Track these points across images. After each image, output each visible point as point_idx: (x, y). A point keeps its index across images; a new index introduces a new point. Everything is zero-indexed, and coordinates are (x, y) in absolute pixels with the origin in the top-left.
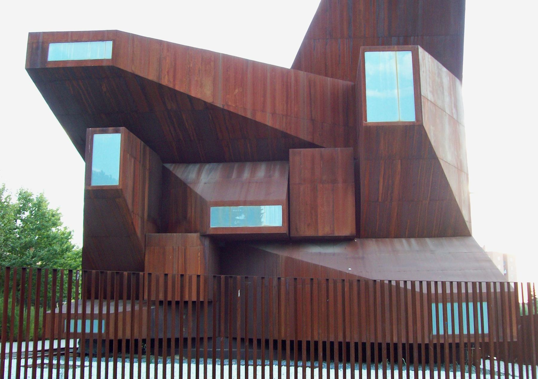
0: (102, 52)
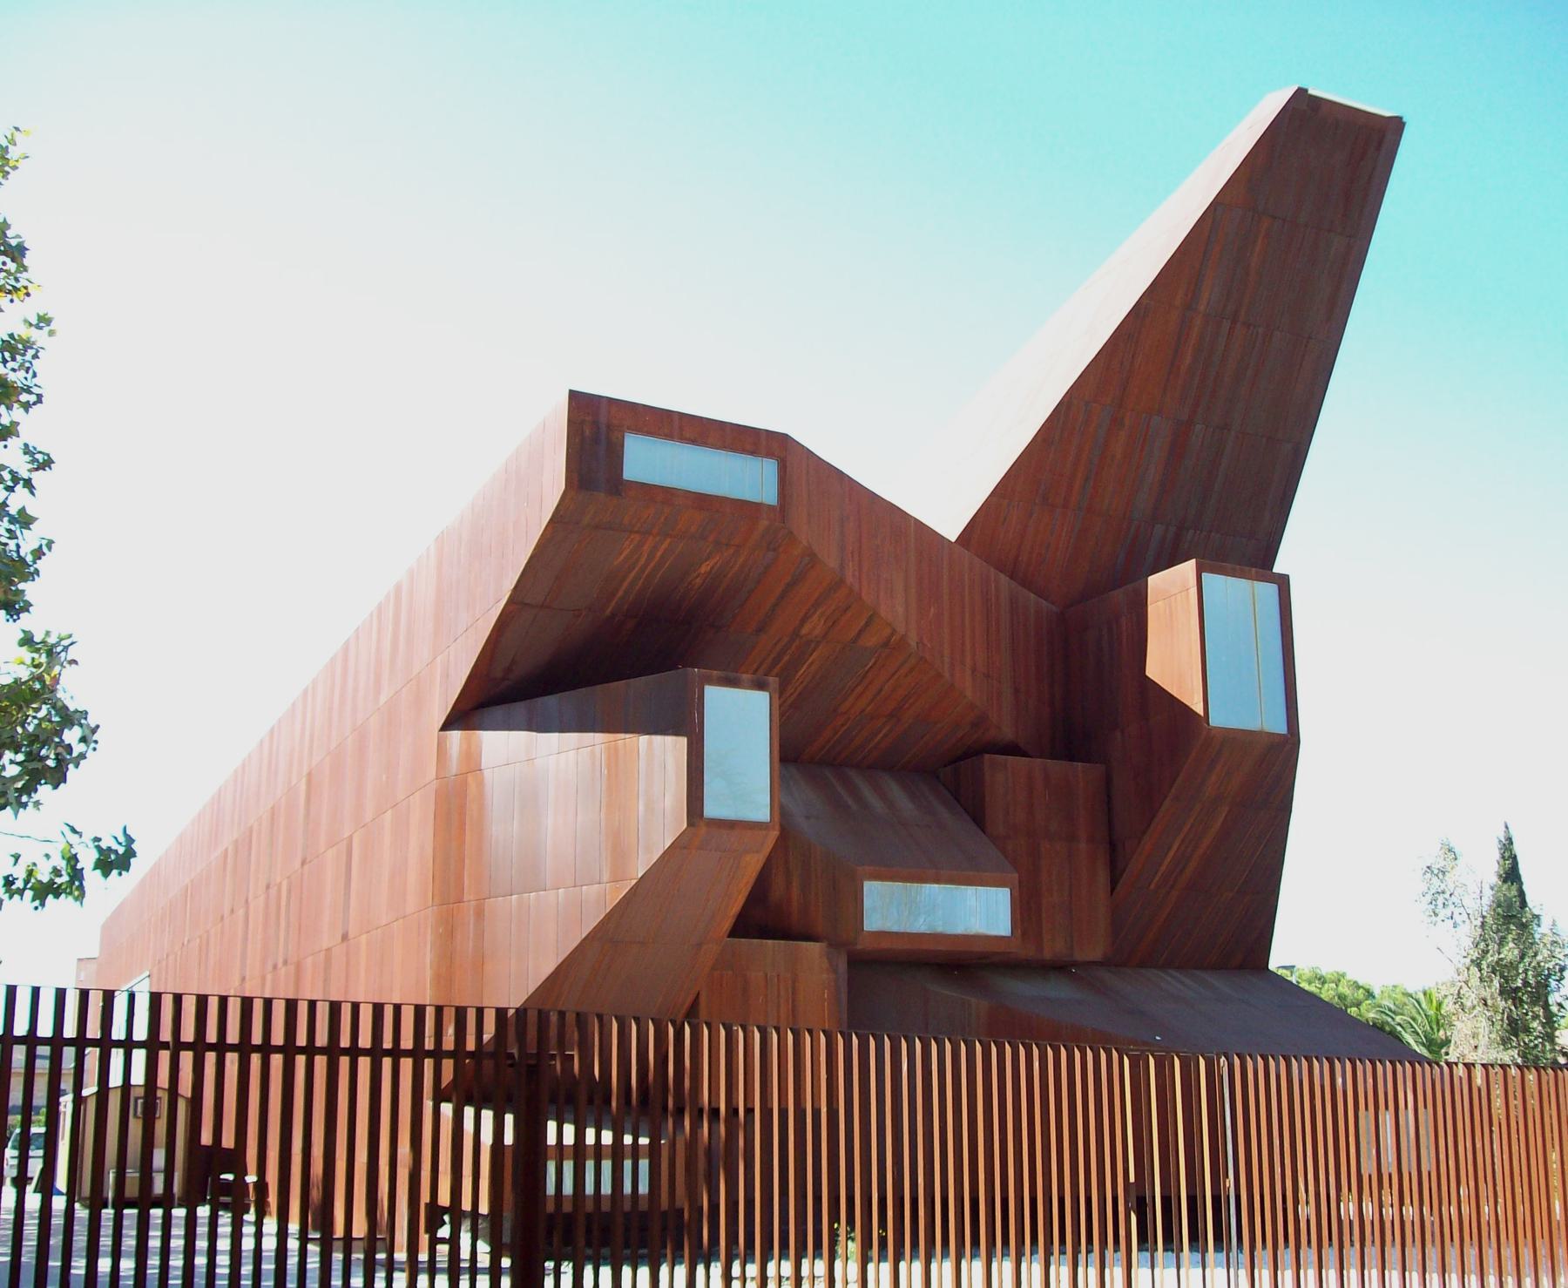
0: (751, 480)
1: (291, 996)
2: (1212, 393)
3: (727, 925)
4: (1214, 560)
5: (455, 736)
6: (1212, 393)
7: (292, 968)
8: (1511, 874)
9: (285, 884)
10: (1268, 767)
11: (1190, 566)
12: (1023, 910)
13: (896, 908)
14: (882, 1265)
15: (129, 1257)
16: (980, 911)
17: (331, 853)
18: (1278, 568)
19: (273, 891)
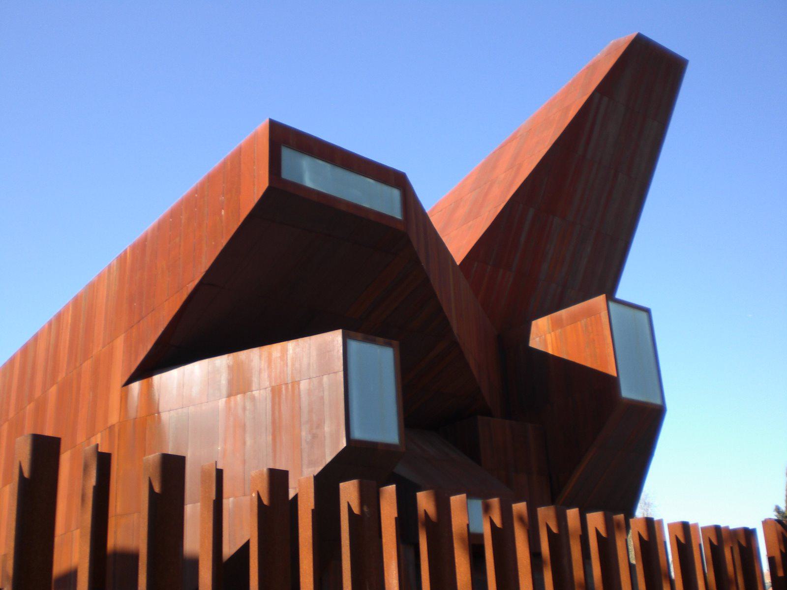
0: (384, 201)
5: (136, 386)
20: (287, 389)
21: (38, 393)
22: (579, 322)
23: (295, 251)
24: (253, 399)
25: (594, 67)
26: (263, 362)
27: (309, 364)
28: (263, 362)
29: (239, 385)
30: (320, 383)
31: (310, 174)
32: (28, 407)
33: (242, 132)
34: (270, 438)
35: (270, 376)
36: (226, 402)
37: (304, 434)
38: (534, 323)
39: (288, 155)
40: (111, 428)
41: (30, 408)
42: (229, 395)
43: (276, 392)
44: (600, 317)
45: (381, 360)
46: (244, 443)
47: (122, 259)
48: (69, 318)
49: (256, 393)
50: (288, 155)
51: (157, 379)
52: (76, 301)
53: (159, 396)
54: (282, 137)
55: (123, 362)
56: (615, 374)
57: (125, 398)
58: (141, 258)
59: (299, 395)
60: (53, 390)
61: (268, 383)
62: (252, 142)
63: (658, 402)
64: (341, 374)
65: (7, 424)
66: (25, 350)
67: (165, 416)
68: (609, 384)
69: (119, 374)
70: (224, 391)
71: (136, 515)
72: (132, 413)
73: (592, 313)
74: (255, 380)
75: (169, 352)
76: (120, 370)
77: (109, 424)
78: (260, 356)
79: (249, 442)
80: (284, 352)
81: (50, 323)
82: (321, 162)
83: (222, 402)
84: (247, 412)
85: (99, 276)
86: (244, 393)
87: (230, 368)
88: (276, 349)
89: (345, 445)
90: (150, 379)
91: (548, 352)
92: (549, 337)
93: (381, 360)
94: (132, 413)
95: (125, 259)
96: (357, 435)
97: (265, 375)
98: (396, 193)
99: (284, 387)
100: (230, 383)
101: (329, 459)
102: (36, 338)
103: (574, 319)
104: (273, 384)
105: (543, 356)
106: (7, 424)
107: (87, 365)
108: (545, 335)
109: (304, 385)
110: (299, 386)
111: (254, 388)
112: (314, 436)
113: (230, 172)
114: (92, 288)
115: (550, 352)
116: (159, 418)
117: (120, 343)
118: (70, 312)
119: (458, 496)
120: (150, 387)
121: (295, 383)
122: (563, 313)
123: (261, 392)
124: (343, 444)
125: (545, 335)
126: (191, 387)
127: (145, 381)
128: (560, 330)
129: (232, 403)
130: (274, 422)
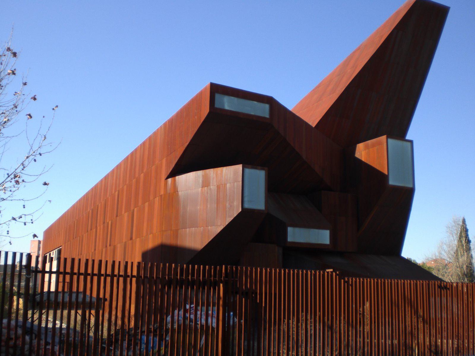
0: (262, 111)
1: (66, 257)
2: (389, 82)
3: (33, 238)
4: (390, 135)
5: (170, 180)
6: (389, 82)
7: (112, 247)
8: (25, 182)
9: (110, 222)
10: (404, 198)
11: (384, 137)
12: (333, 237)
13: (296, 235)
14: (367, 303)
15: (64, 328)
16: (323, 237)
17: (126, 214)
18: (408, 137)
19: (106, 225)
20: (222, 186)
21: (137, 175)
22: (375, 147)
23: (225, 130)
24: (211, 189)
25: (398, 13)
26: (214, 175)
27: (230, 177)
28: (214, 175)
29: (206, 183)
30: (234, 185)
31: (228, 104)
32: (133, 181)
33: (199, 85)
34: (216, 205)
35: (217, 181)
36: (201, 190)
37: (227, 204)
38: (358, 145)
39: (217, 96)
40: (161, 196)
41: (134, 181)
42: (202, 187)
43: (218, 187)
44: (384, 146)
45: (259, 176)
46: (207, 207)
47: (165, 124)
48: (147, 146)
49: (212, 187)
50: (217, 96)
51: (177, 177)
52: (150, 138)
53: (178, 185)
54: (216, 90)
55: (165, 171)
56: (387, 174)
57: (166, 184)
58: (172, 126)
59: (226, 189)
60: (142, 175)
61: (216, 183)
62: (206, 88)
63: (411, 186)
64: (241, 182)
65: (126, 186)
66: (132, 154)
67: (180, 193)
68: (382, 178)
69: (164, 175)
70: (201, 186)
71: (169, 231)
72: (168, 191)
73: (380, 143)
74: (211, 182)
75: (181, 168)
76: (164, 173)
77: (161, 194)
78: (214, 172)
79: (209, 206)
80: (222, 171)
81: (141, 145)
82: (233, 98)
83: (200, 189)
84: (208, 194)
85: (158, 130)
86: (207, 186)
87: (203, 176)
88: (219, 169)
89: (241, 210)
90: (175, 177)
91: (362, 159)
92: (363, 153)
93: (259, 176)
94: (168, 191)
95: (166, 124)
96: (246, 206)
97: (215, 180)
98: (267, 106)
99: (221, 185)
100: (203, 182)
101: (235, 215)
102: (136, 150)
103: (373, 146)
104: (218, 184)
105: (360, 161)
106: (126, 186)
107: (153, 167)
108: (363, 151)
109: (228, 185)
110: (226, 185)
111: (211, 185)
112: (231, 206)
113: (196, 101)
114: (155, 134)
115: (363, 160)
116: (178, 193)
117: (164, 161)
118: (148, 142)
119: (134, 278)
120: (175, 181)
121: (226, 184)
122: (369, 142)
123: (213, 187)
124: (240, 210)
125: (363, 151)
126: (189, 181)
127: (173, 178)
128: (367, 150)
129: (203, 190)
130: (217, 199)
